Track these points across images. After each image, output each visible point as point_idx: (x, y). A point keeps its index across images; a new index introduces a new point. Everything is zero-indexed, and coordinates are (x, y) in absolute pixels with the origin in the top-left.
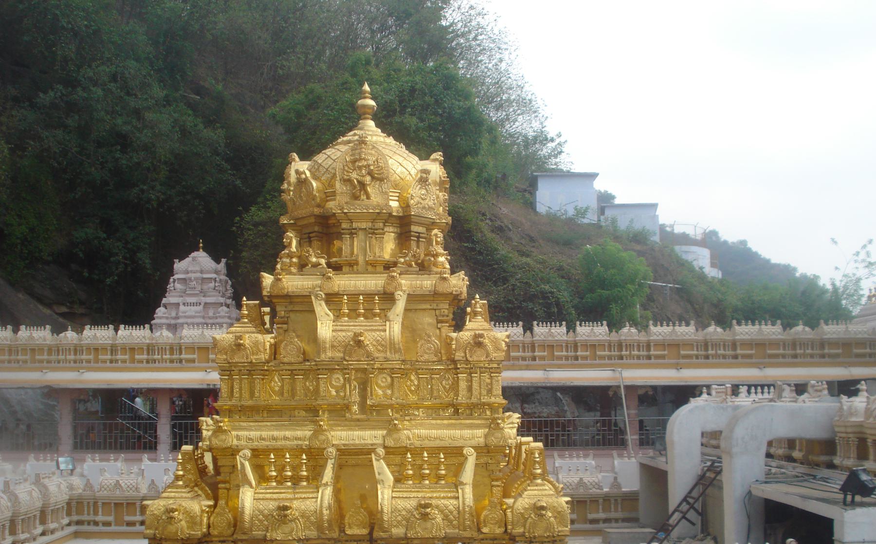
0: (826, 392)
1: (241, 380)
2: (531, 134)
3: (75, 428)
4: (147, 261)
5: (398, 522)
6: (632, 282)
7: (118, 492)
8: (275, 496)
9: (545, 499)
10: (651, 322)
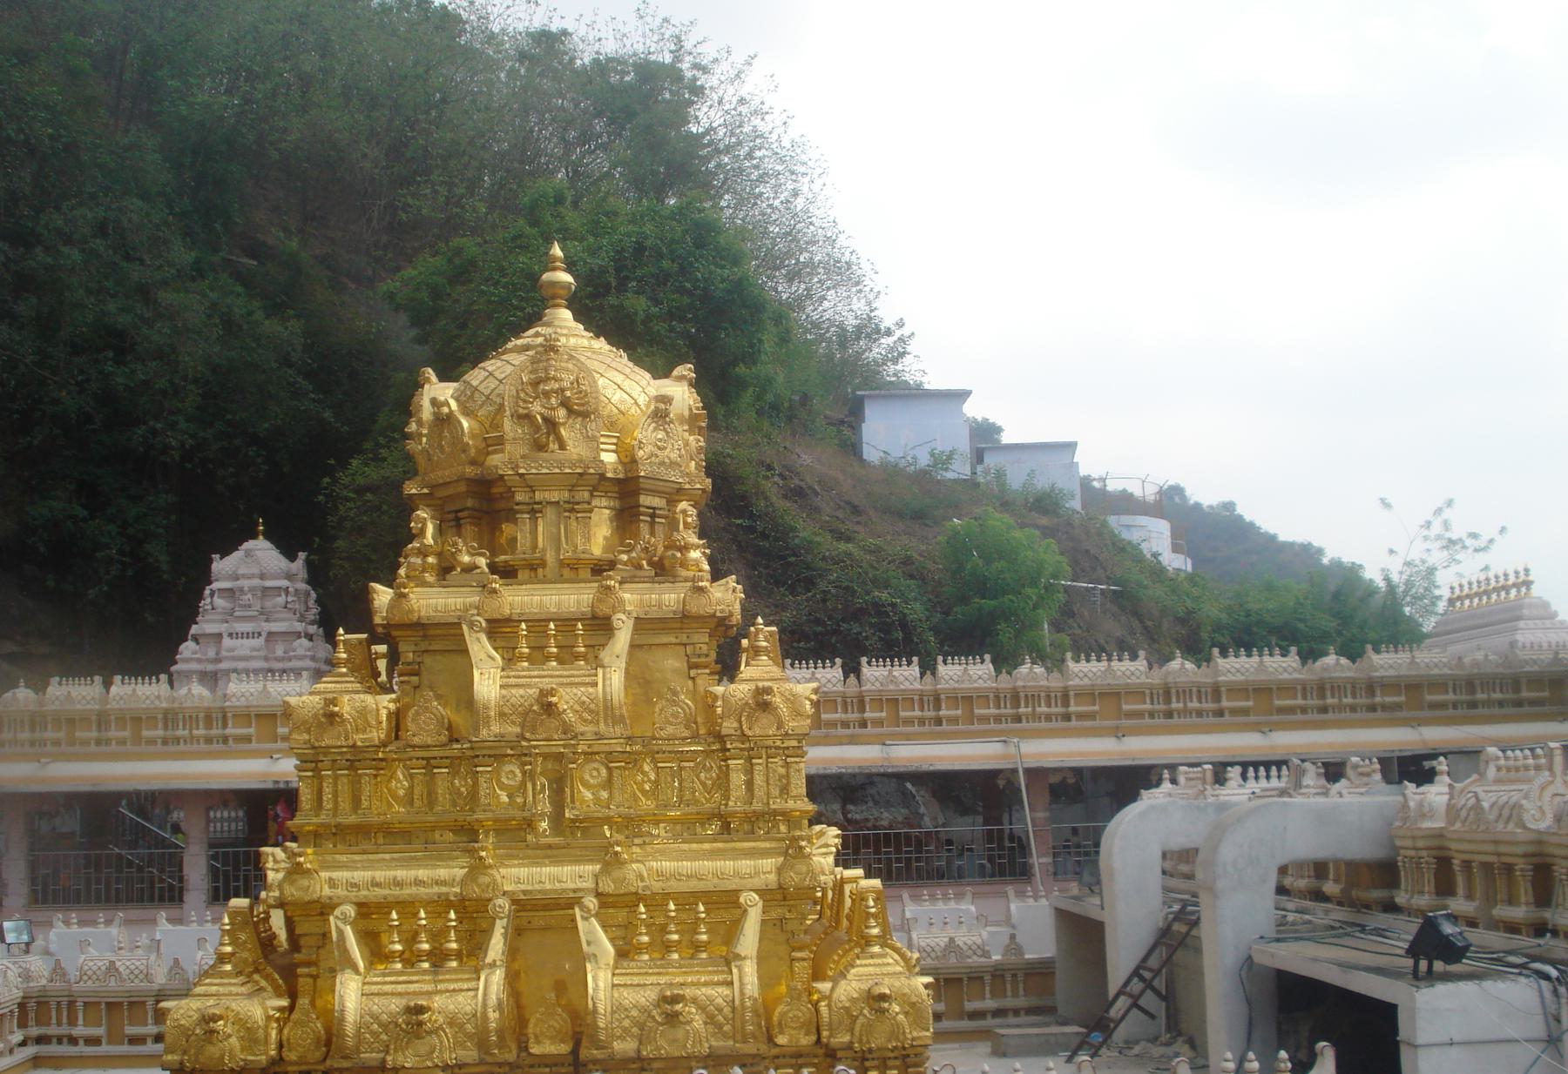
0: (1378, 776)
1: (336, 778)
2: (851, 322)
3: (33, 867)
4: (163, 558)
5: (625, 1029)
6: (1034, 583)
7: (113, 983)
8: (400, 988)
9: (887, 981)
10: (1069, 655)
